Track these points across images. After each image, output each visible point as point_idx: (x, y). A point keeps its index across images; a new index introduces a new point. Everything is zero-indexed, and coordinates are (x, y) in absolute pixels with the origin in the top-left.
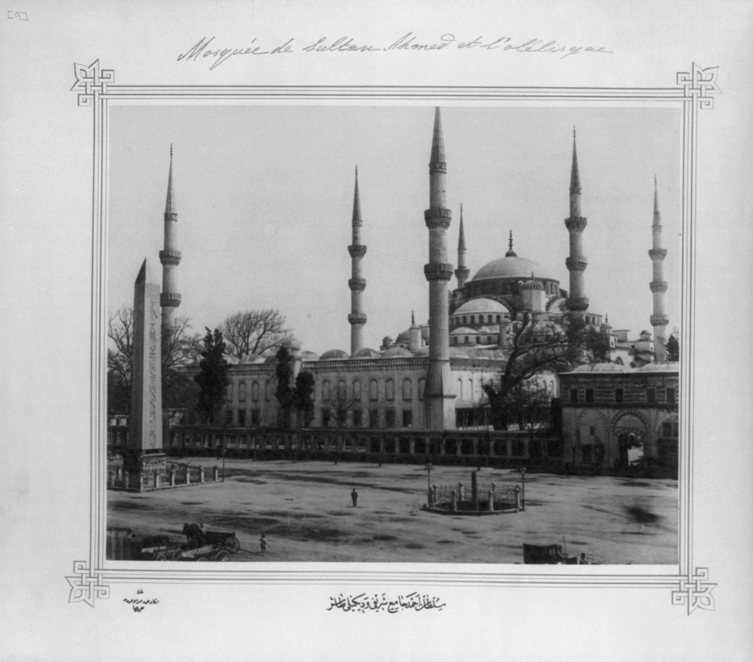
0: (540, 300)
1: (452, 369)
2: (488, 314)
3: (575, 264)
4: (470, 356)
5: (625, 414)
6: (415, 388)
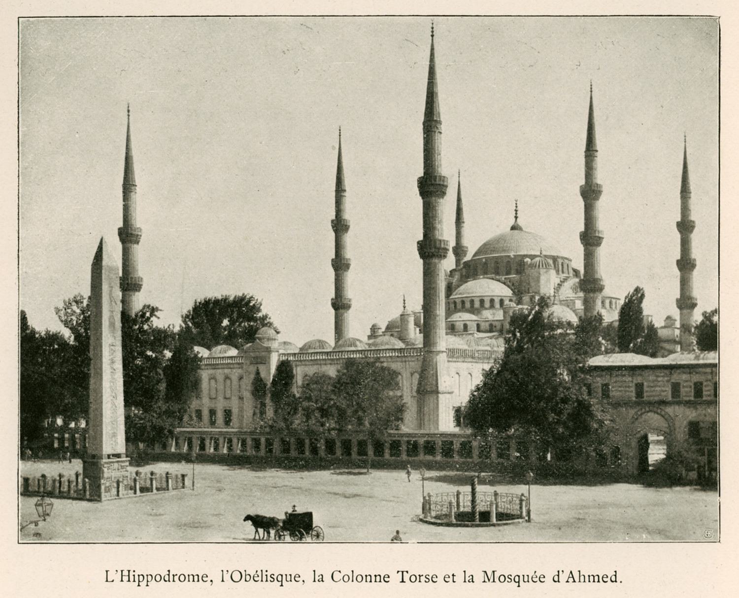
3: (590, 239)
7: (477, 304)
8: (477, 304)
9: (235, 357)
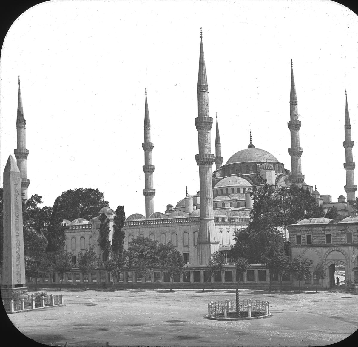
0: (272, 177)
1: (216, 225)
2: (237, 188)
3: (295, 152)
4: (227, 216)
5: (333, 251)
6: (191, 238)
7: (230, 191)
8: (230, 191)
9: (87, 225)
